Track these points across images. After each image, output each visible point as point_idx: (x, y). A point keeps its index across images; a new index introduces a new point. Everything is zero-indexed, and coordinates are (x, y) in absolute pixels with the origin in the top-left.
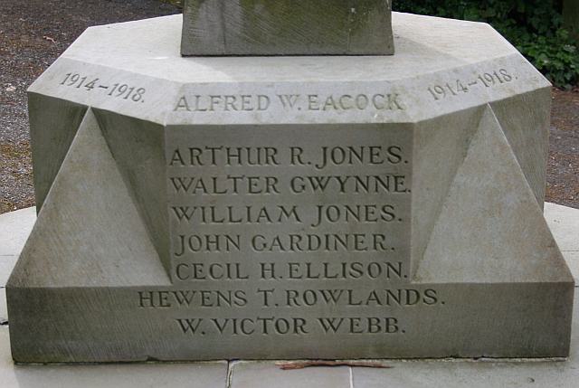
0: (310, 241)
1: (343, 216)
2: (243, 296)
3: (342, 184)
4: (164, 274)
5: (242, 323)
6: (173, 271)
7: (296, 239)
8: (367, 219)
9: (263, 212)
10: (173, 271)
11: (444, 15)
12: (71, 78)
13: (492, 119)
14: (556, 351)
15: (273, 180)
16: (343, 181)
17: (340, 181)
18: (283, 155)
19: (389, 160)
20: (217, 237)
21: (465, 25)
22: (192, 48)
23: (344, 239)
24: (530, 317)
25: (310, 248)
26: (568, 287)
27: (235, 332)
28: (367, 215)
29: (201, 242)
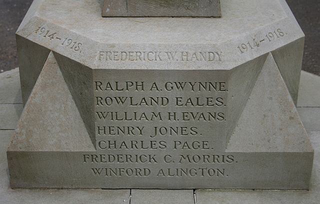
0: (162, 101)
3: (141, 131)
4: (90, 142)
5: (140, 157)
6: (97, 144)
7: (138, 170)
8: (203, 148)
9: (143, 115)
10: (97, 144)
15: (208, 157)
16: (193, 85)
17: (191, 84)
18: (148, 86)
20: (175, 113)
23: (156, 100)
25: (163, 104)
27: (137, 161)
28: (203, 146)
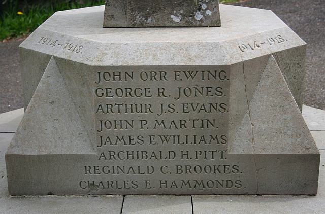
1: (193, 94)
2: (142, 139)
11: (250, 5)
12: (45, 40)
13: (275, 68)
14: (308, 189)
19: (233, 172)
21: (254, 10)
22: (109, 22)
24: (295, 173)
26: (315, 158)
29: (147, 76)
